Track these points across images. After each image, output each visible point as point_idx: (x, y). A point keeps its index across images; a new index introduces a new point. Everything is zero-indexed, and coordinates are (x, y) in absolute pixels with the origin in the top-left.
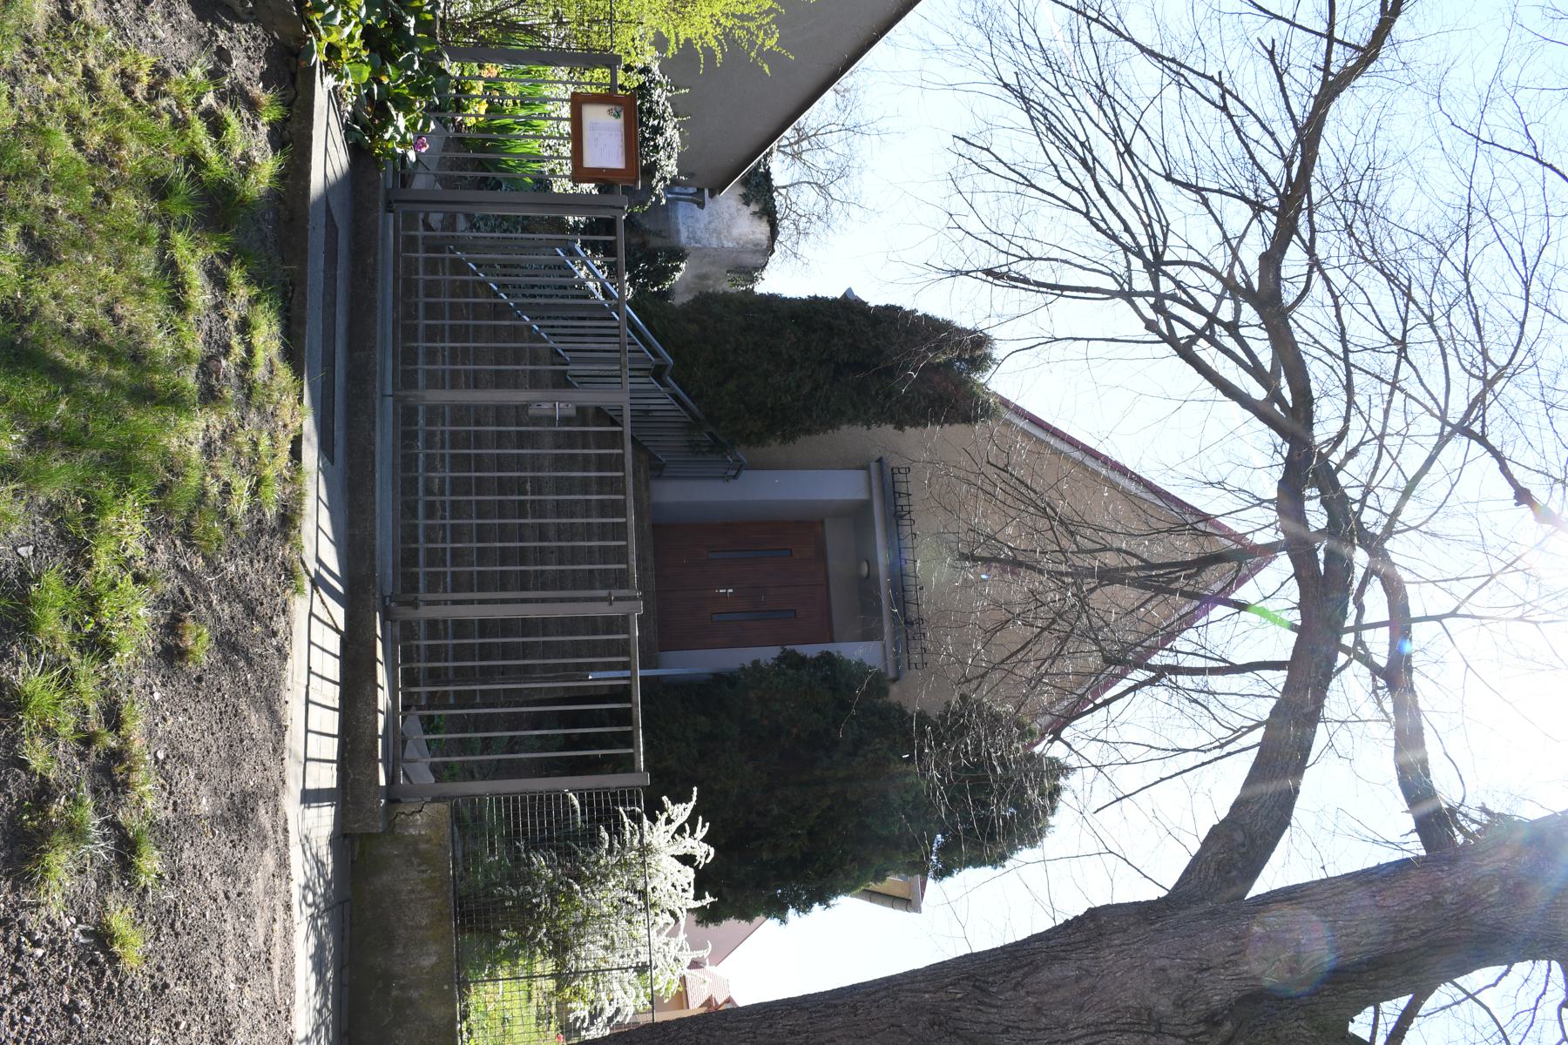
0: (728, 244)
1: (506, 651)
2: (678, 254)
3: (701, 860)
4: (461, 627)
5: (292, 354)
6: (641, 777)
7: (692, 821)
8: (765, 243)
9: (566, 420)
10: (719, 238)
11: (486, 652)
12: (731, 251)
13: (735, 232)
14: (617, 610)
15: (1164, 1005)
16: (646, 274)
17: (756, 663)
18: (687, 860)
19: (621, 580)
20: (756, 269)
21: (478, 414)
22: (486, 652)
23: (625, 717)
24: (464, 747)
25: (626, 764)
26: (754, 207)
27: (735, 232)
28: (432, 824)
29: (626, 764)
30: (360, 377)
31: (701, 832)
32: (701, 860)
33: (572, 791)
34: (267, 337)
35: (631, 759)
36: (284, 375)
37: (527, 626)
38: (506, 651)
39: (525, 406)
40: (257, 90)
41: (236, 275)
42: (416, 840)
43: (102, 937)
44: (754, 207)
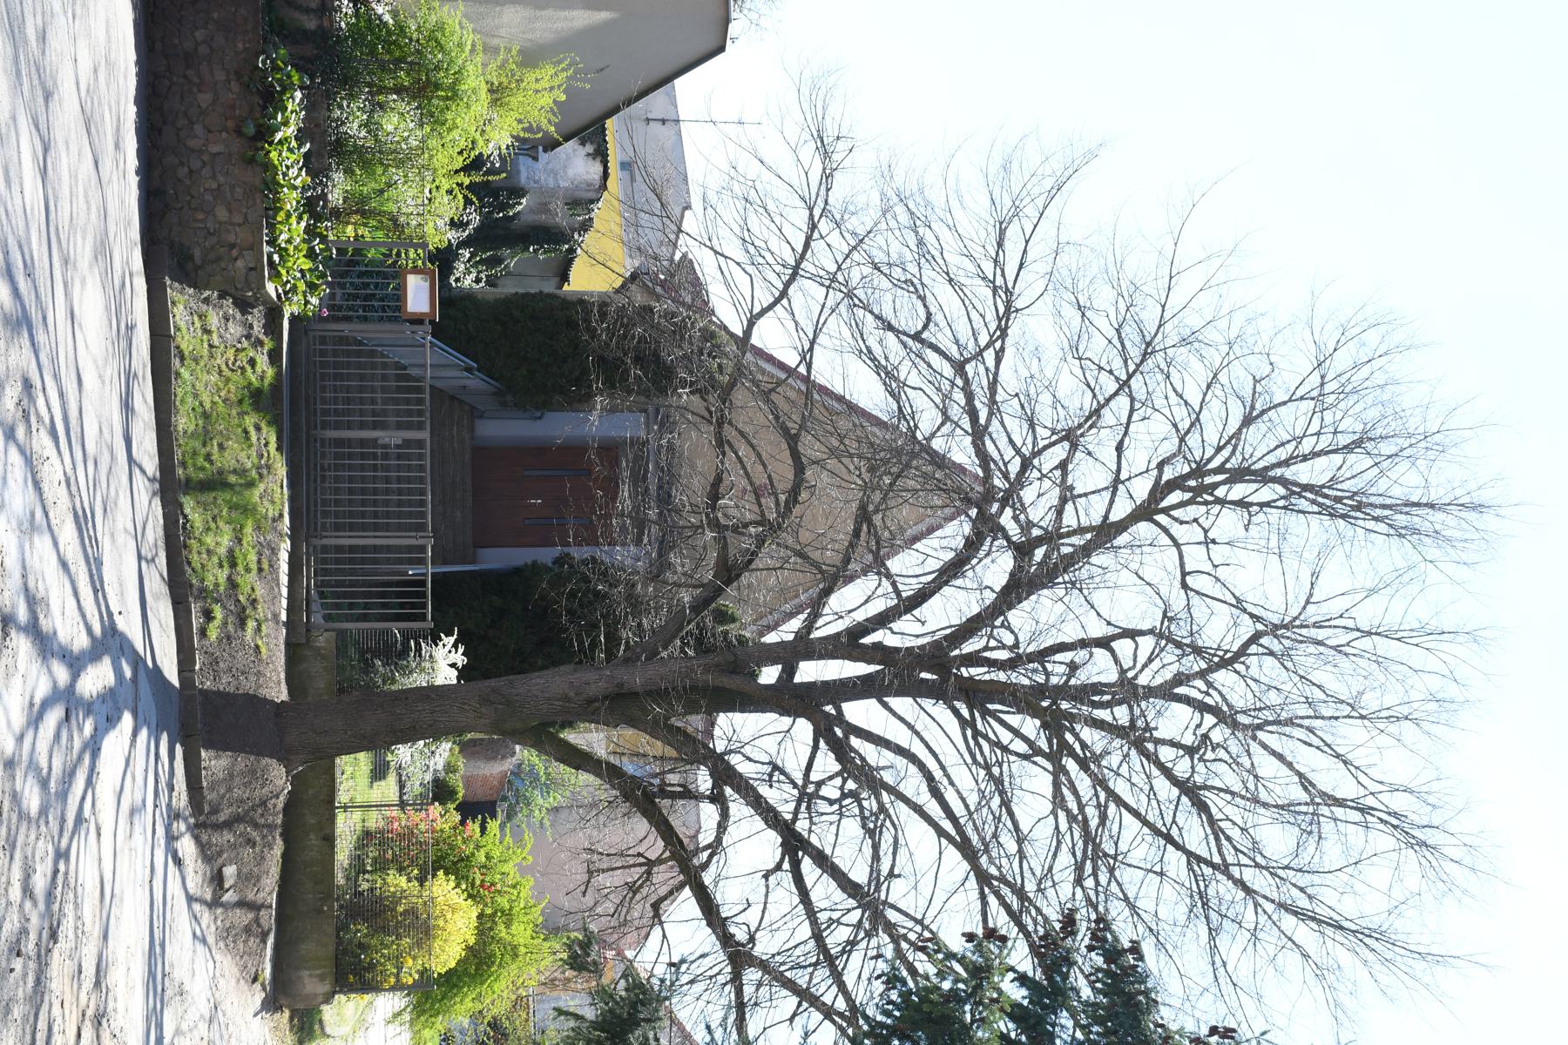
0: (563, 184)
1: (363, 561)
2: (519, 192)
3: (460, 665)
4: (339, 549)
5: (279, 449)
6: (429, 624)
7: (455, 646)
8: (597, 183)
9: (398, 446)
10: (556, 179)
11: (351, 561)
12: (566, 189)
13: (571, 173)
14: (421, 542)
15: (572, 694)
16: (490, 205)
17: (534, 562)
18: (453, 665)
19: (422, 527)
20: (592, 202)
21: (349, 443)
22: (351, 561)
23: (423, 595)
24: (338, 606)
25: (423, 618)
26: (590, 148)
27: (571, 173)
28: (327, 641)
29: (423, 618)
30: (295, 429)
31: (461, 650)
32: (460, 665)
33: (396, 629)
34: (273, 439)
35: (424, 615)
36: (278, 456)
37: (376, 549)
38: (363, 561)
39: (376, 440)
40: (262, 337)
41: (263, 425)
42: (319, 648)
43: (257, 647)
44: (590, 148)
